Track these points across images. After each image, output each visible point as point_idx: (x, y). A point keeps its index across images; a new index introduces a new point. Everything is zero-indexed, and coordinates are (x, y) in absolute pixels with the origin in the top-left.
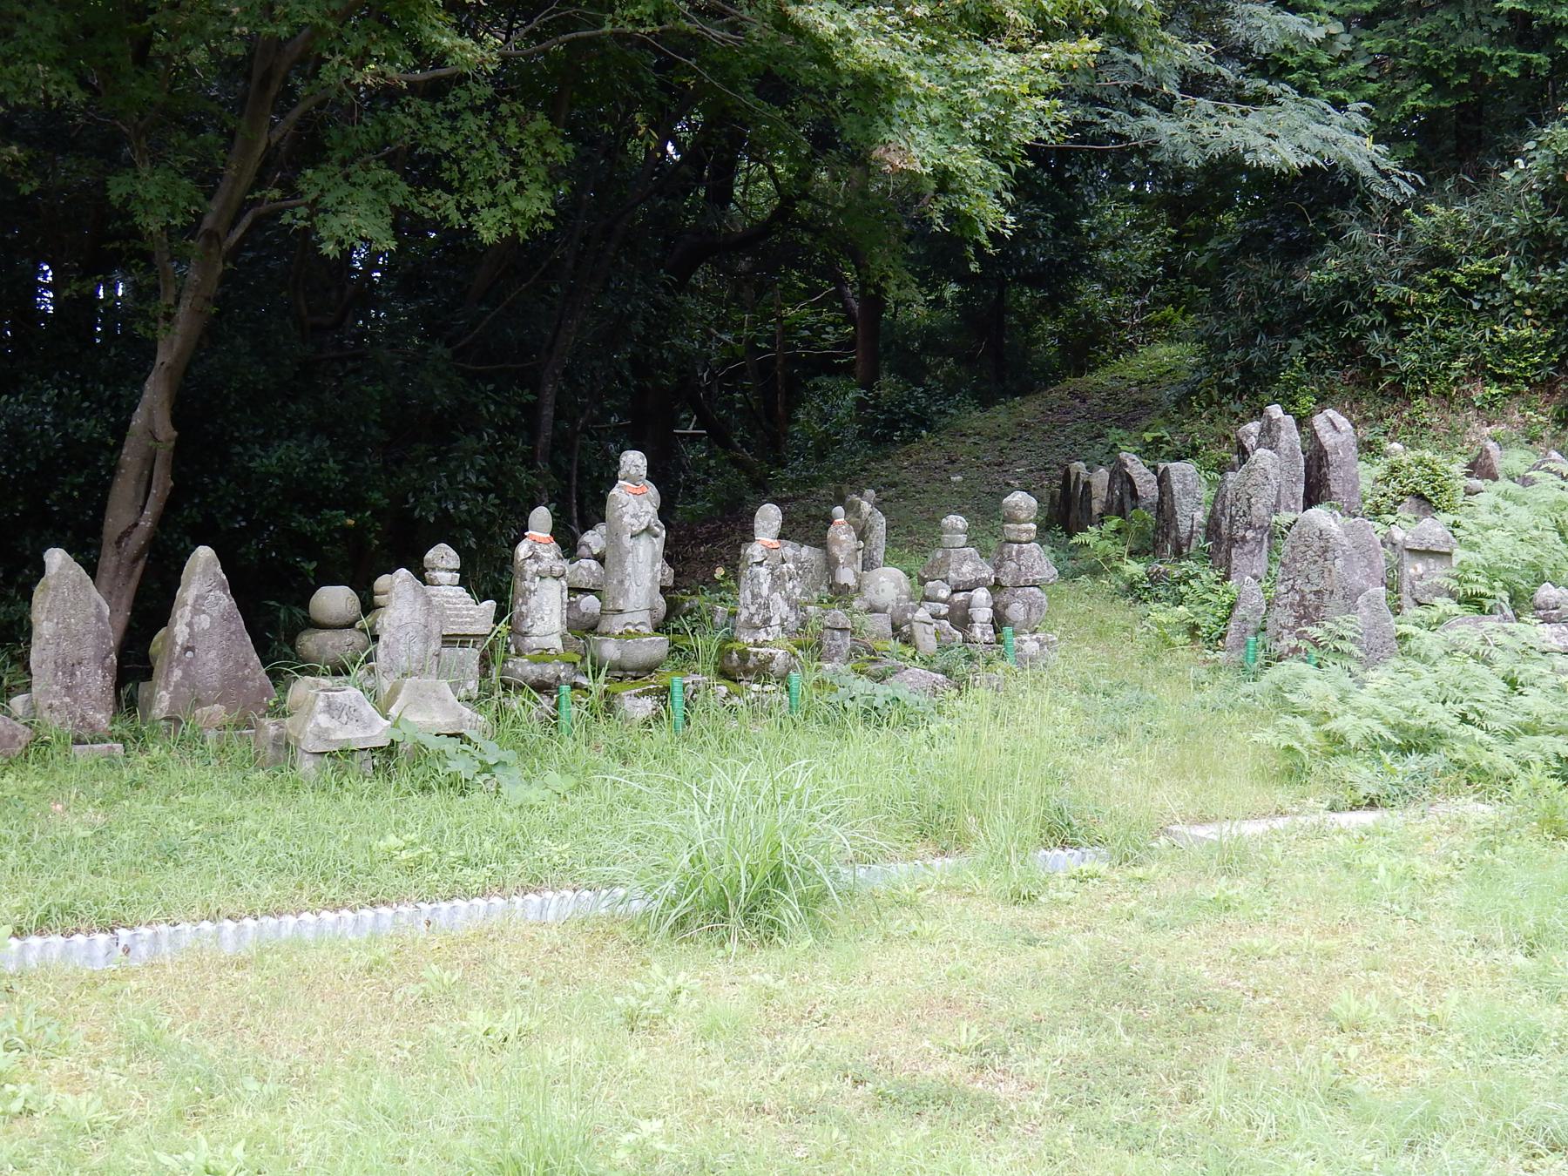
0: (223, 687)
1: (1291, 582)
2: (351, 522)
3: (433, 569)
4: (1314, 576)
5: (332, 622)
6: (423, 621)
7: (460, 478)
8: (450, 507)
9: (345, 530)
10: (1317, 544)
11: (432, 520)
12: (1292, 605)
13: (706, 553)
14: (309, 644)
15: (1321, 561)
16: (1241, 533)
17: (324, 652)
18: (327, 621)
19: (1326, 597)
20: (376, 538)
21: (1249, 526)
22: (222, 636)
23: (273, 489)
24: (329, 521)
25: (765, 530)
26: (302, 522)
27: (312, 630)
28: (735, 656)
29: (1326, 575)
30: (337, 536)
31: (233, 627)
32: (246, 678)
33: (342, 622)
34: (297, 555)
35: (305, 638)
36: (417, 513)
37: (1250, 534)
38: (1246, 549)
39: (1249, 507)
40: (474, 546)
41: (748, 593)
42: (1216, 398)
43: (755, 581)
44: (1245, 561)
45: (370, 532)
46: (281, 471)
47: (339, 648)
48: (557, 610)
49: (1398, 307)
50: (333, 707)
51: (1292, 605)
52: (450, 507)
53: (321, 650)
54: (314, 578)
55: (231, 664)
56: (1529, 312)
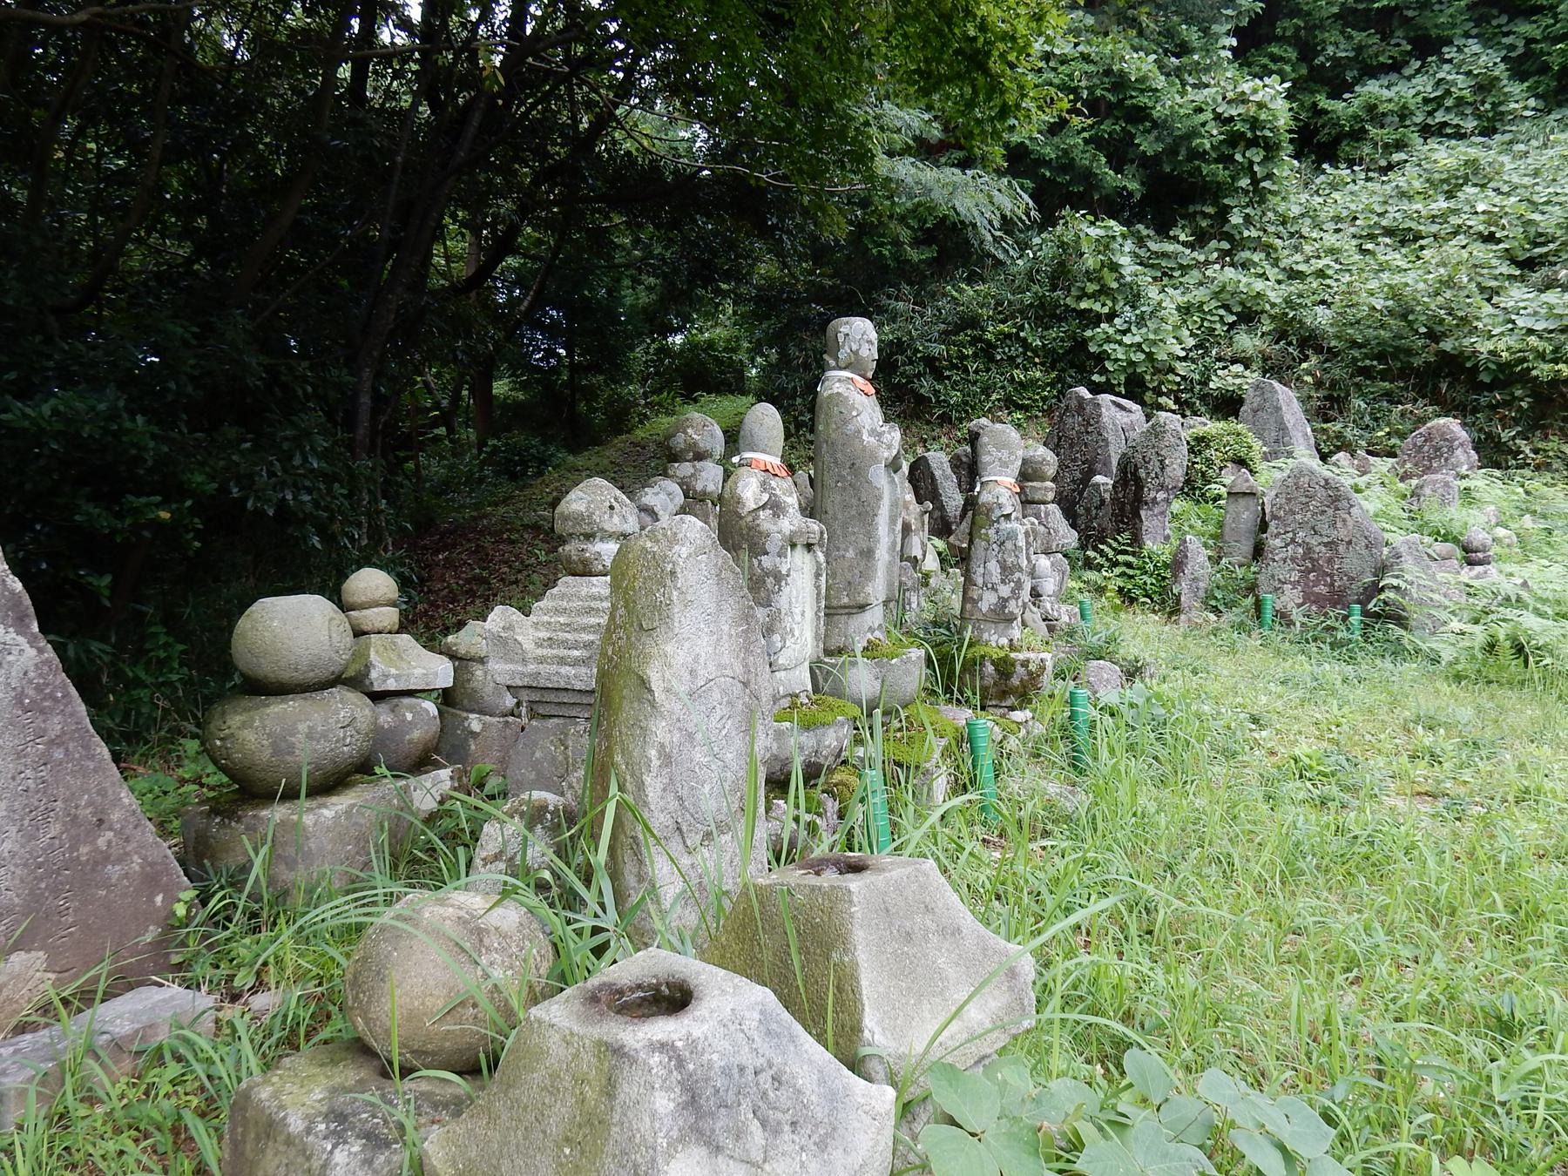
0: (35, 898)
1: (1290, 535)
2: (165, 515)
3: (589, 537)
4: (1324, 528)
5: (298, 677)
6: (739, 669)
7: (297, 461)
8: (289, 497)
9: (157, 525)
10: (1321, 493)
11: (271, 513)
12: (1293, 559)
13: (446, 559)
14: (249, 736)
15: (1330, 512)
16: (1153, 494)
17: (291, 749)
18: (286, 676)
19: (1341, 548)
20: (195, 539)
21: (1162, 487)
22: (20, 755)
23: (42, 462)
24: (136, 511)
25: (1005, 465)
26: (90, 513)
27: (247, 702)
28: (990, 669)
29: (1339, 525)
30: (146, 534)
31: (55, 725)
32: (105, 858)
33: (323, 674)
34: (81, 568)
35: (235, 720)
36: (250, 505)
37: (1161, 496)
38: (1156, 511)
39: (1162, 469)
40: (319, 546)
41: (993, 566)
42: (793, 431)
43: (1009, 545)
44: (1155, 522)
45: (188, 532)
46: (59, 426)
47: (324, 736)
48: (809, 614)
49: (937, 359)
50: (708, 1101)
51: (1293, 559)
52: (289, 497)
53: (281, 746)
54: (109, 599)
55: (55, 829)
56: (1037, 360)
